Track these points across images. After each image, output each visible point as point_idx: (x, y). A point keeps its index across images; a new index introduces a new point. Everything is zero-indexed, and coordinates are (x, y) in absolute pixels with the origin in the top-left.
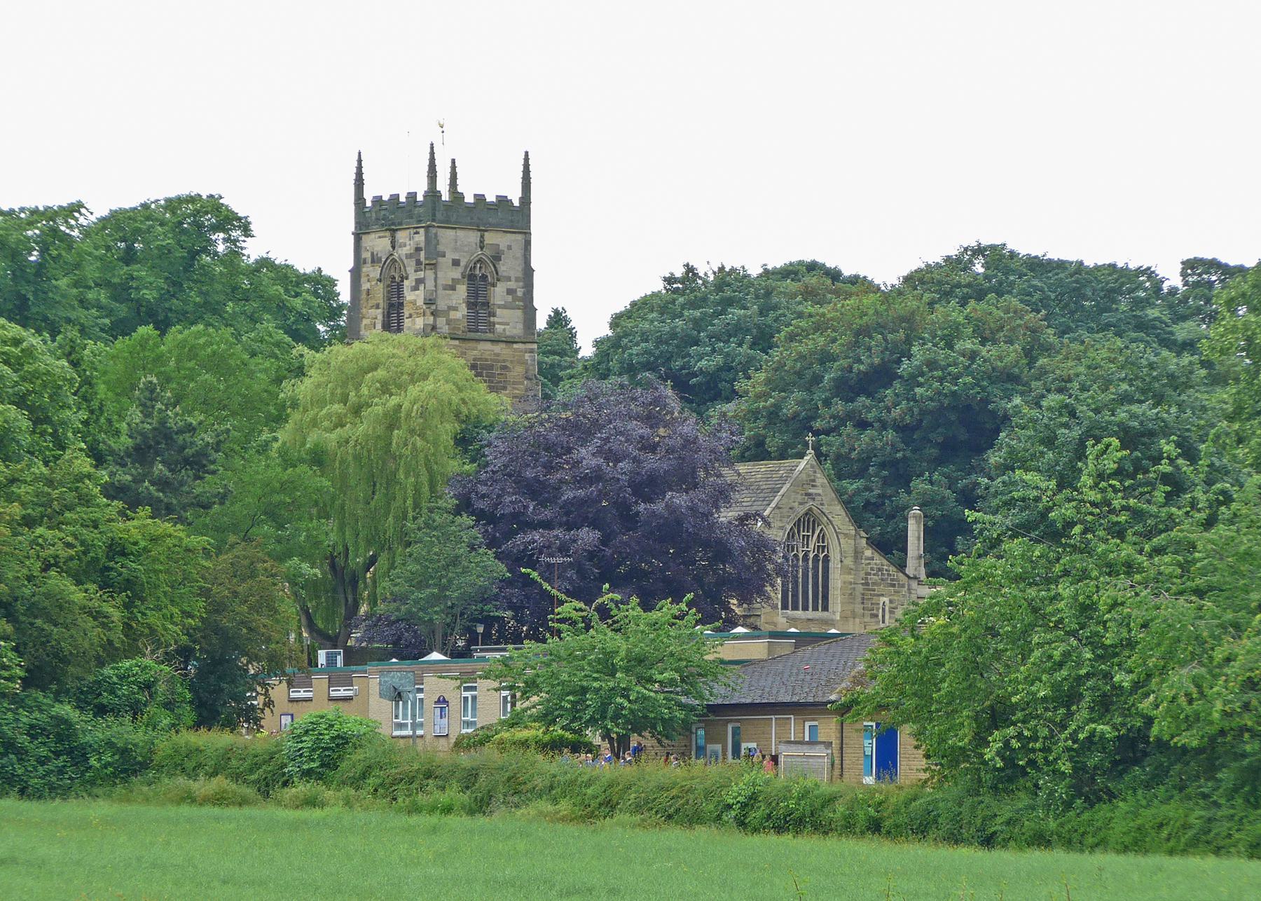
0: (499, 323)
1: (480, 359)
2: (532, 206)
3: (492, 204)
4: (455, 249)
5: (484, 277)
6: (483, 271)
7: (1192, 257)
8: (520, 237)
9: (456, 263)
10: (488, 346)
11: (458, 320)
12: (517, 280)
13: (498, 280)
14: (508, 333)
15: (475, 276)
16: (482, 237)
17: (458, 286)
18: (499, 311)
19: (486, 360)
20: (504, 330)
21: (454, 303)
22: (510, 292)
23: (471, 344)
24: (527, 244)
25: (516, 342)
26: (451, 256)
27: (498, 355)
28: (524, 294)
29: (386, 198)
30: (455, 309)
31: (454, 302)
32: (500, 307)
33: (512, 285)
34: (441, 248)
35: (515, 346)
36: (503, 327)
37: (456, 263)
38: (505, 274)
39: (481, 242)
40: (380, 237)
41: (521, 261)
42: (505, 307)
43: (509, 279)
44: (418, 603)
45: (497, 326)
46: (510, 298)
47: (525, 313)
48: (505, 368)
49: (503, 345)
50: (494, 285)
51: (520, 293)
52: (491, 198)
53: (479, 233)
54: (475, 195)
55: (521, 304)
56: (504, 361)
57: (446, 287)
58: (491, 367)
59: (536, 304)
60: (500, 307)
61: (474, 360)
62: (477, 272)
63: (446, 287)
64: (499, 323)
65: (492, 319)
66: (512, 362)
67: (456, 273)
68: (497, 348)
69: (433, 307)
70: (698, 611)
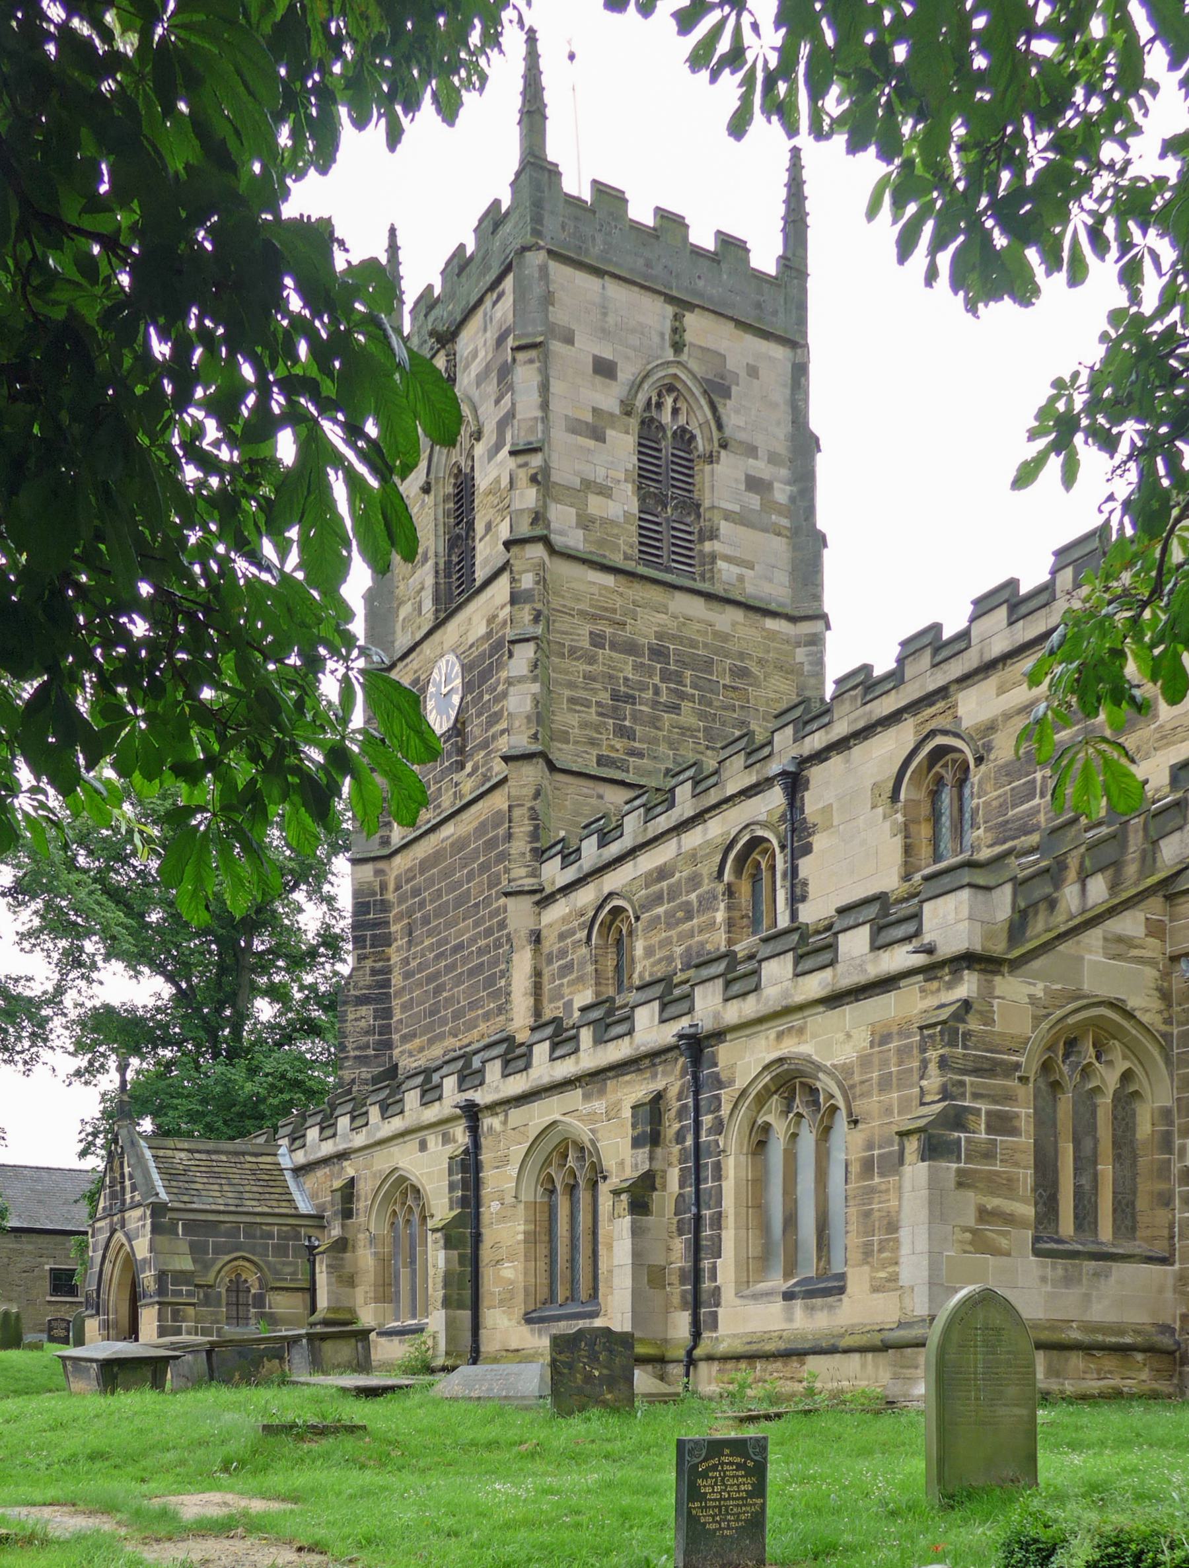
0: (728, 559)
1: (674, 638)
2: (811, 284)
3: (636, 227)
4: (604, 333)
5: (684, 437)
6: (682, 420)
7: (339, 155)
8: (778, 352)
9: (604, 369)
10: (695, 607)
11: (612, 523)
12: (773, 459)
13: (724, 445)
14: (750, 589)
15: (661, 427)
16: (677, 317)
17: (610, 433)
18: (725, 527)
19: (693, 644)
20: (741, 578)
21: (599, 475)
22: (754, 484)
23: (654, 594)
24: (800, 371)
25: (774, 614)
26: (588, 347)
27: (725, 637)
28: (792, 499)
29: (702, 237)
30: (605, 492)
31: (601, 472)
32: (728, 516)
33: (760, 468)
34: (559, 315)
35: (771, 624)
36: (735, 570)
37: (604, 369)
38: (742, 436)
39: (675, 331)
40: (495, 303)
41: (783, 414)
42: (740, 519)
43: (751, 451)
44: (887, 1504)
45: (721, 564)
46: (754, 501)
47: (795, 548)
48: (742, 673)
49: (738, 615)
50: (711, 459)
51: (781, 493)
52: (641, 212)
53: (670, 310)
54: (719, 233)
55: (785, 522)
56: (742, 656)
57: (576, 427)
58: (708, 664)
59: (822, 523)
60: (728, 516)
61: (660, 636)
62: (666, 417)
63: (576, 427)
64: (728, 559)
65: (708, 546)
66: (760, 661)
67: (608, 398)
68: (727, 619)
69: (536, 461)
70: (276, 532)
